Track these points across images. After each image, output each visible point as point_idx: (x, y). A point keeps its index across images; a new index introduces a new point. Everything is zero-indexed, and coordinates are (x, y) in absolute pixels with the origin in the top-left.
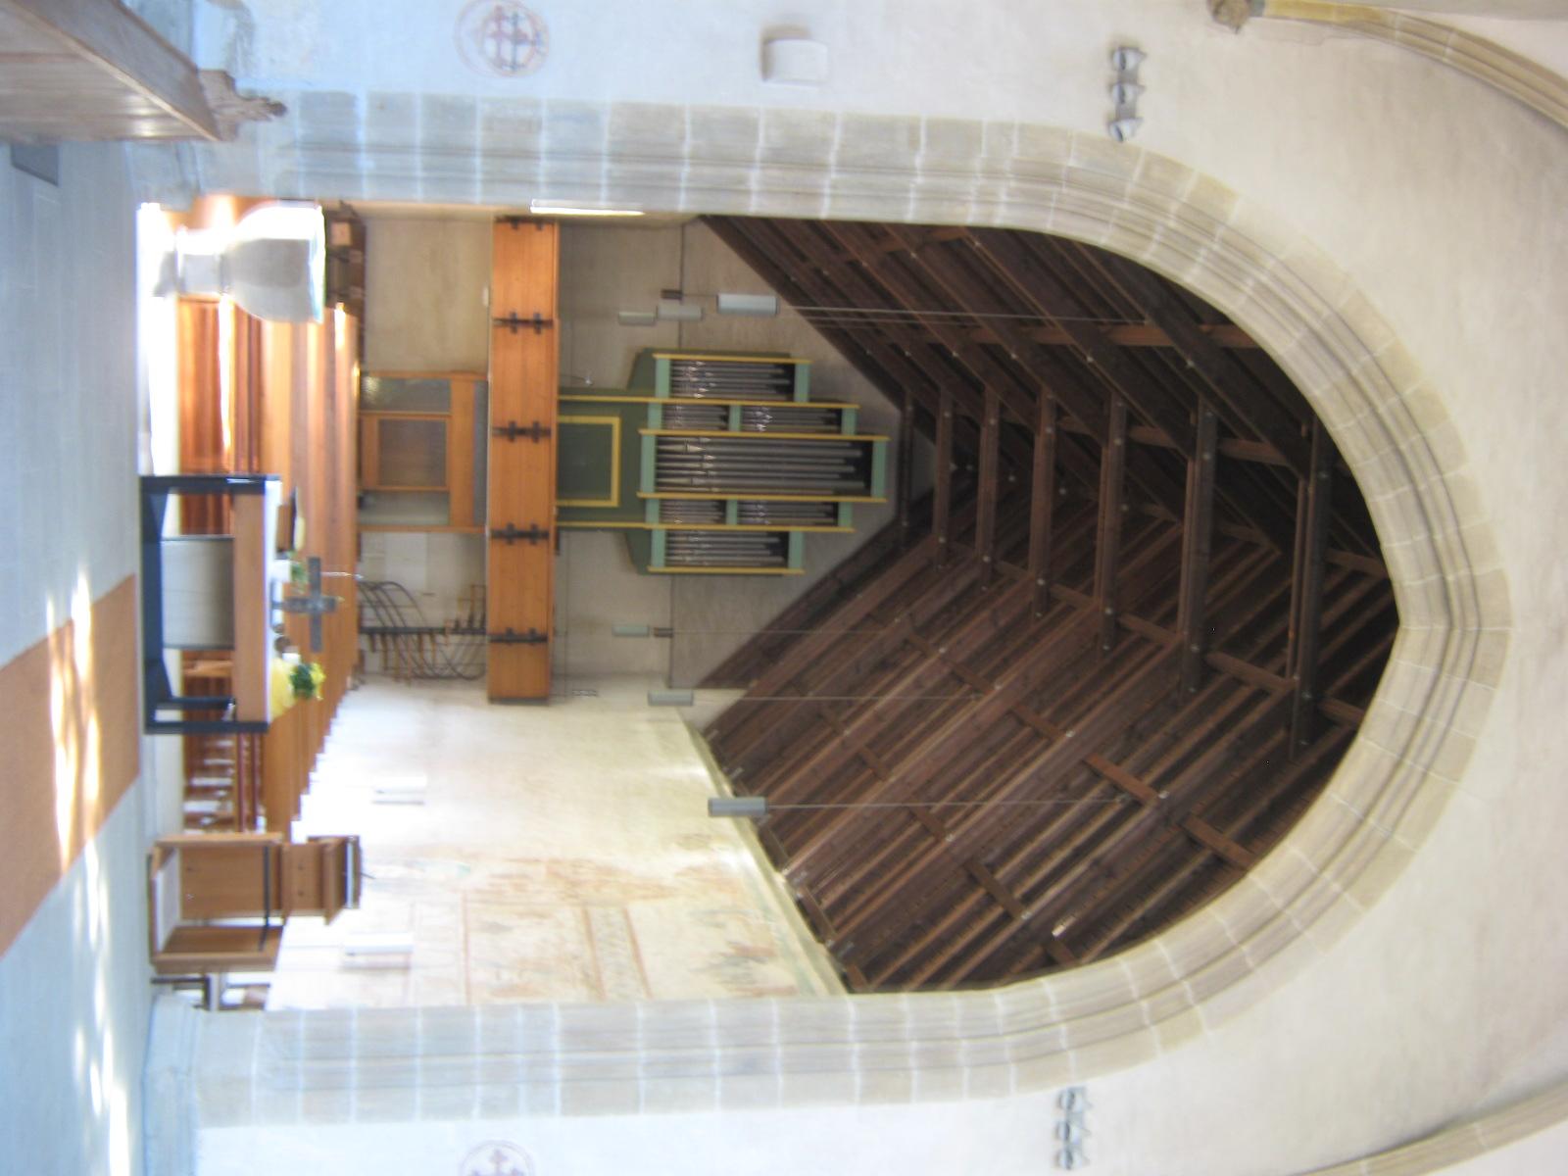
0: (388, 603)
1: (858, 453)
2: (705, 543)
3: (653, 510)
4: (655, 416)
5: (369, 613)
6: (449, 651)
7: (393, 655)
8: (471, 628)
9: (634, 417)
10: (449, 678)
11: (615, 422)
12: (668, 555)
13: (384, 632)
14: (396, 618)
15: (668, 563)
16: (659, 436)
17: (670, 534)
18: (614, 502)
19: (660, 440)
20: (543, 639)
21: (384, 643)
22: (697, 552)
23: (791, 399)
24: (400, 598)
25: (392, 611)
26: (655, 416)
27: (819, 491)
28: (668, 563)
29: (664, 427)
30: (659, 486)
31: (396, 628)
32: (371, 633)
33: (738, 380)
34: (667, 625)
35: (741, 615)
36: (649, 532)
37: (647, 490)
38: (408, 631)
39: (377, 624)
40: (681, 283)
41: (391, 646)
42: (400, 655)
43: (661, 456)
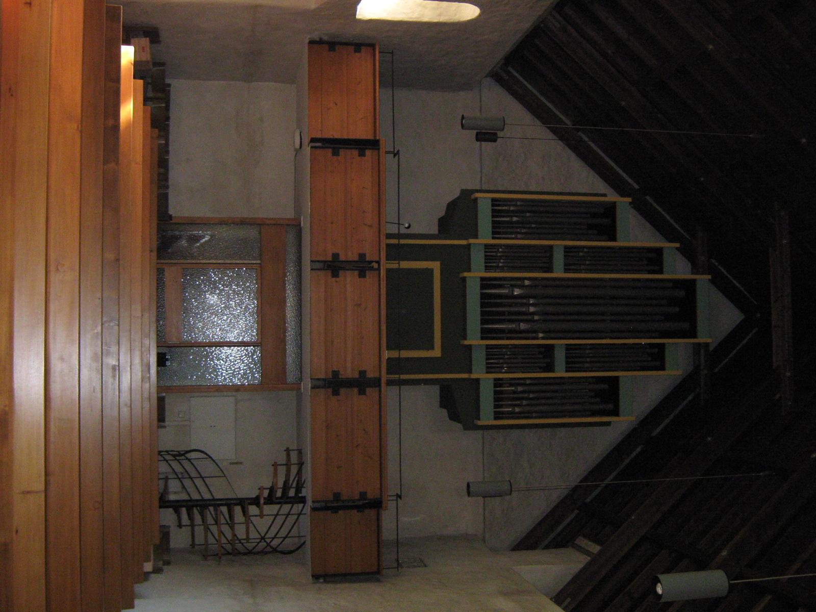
0: (194, 474)
1: (681, 293)
2: (533, 392)
3: (479, 359)
4: (478, 258)
5: (174, 485)
6: (262, 524)
7: (199, 531)
8: (284, 495)
9: (455, 262)
10: (263, 553)
11: (435, 266)
12: (496, 406)
13: (190, 505)
14: (203, 489)
15: (497, 416)
16: (482, 279)
17: (498, 383)
18: (437, 352)
19: (486, 283)
20: (377, 504)
21: (191, 517)
22: (524, 402)
23: (614, 239)
24: (207, 469)
25: (199, 482)
26: (478, 258)
27: (649, 334)
28: (497, 416)
29: (487, 268)
30: (486, 334)
31: (203, 500)
32: (176, 506)
33: (494, 309)
34: (160, 429)
35: (560, 458)
36: (477, 381)
37: (474, 339)
38: (216, 503)
39: (184, 497)
40: (381, 494)
41: (198, 519)
42: (207, 529)
43: (486, 300)
